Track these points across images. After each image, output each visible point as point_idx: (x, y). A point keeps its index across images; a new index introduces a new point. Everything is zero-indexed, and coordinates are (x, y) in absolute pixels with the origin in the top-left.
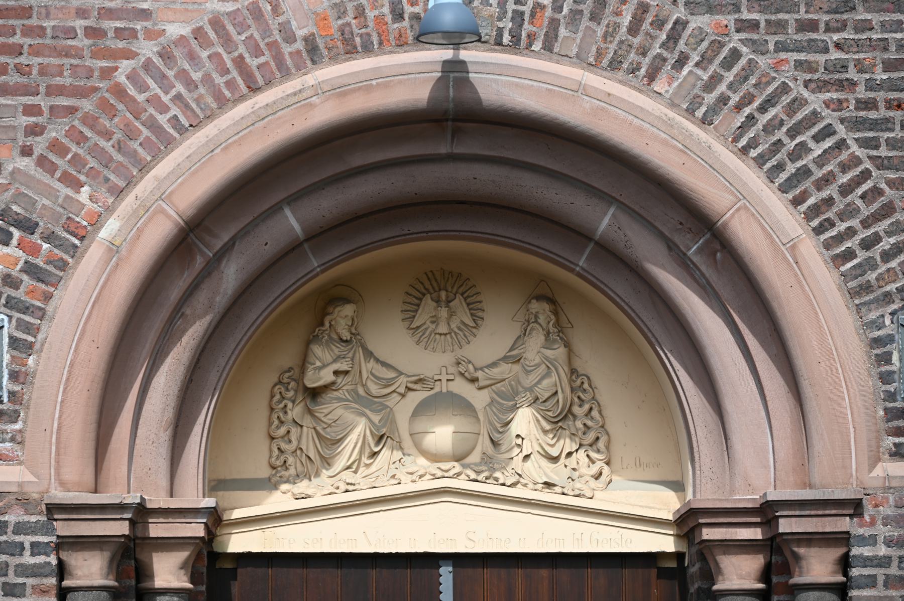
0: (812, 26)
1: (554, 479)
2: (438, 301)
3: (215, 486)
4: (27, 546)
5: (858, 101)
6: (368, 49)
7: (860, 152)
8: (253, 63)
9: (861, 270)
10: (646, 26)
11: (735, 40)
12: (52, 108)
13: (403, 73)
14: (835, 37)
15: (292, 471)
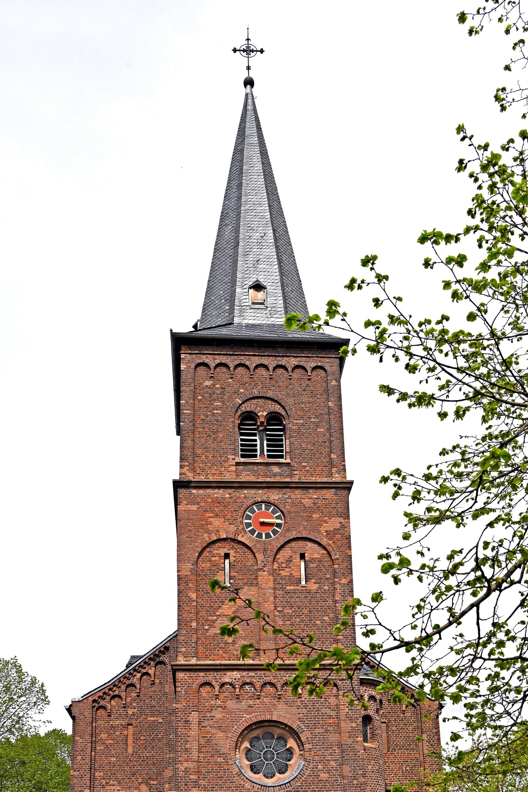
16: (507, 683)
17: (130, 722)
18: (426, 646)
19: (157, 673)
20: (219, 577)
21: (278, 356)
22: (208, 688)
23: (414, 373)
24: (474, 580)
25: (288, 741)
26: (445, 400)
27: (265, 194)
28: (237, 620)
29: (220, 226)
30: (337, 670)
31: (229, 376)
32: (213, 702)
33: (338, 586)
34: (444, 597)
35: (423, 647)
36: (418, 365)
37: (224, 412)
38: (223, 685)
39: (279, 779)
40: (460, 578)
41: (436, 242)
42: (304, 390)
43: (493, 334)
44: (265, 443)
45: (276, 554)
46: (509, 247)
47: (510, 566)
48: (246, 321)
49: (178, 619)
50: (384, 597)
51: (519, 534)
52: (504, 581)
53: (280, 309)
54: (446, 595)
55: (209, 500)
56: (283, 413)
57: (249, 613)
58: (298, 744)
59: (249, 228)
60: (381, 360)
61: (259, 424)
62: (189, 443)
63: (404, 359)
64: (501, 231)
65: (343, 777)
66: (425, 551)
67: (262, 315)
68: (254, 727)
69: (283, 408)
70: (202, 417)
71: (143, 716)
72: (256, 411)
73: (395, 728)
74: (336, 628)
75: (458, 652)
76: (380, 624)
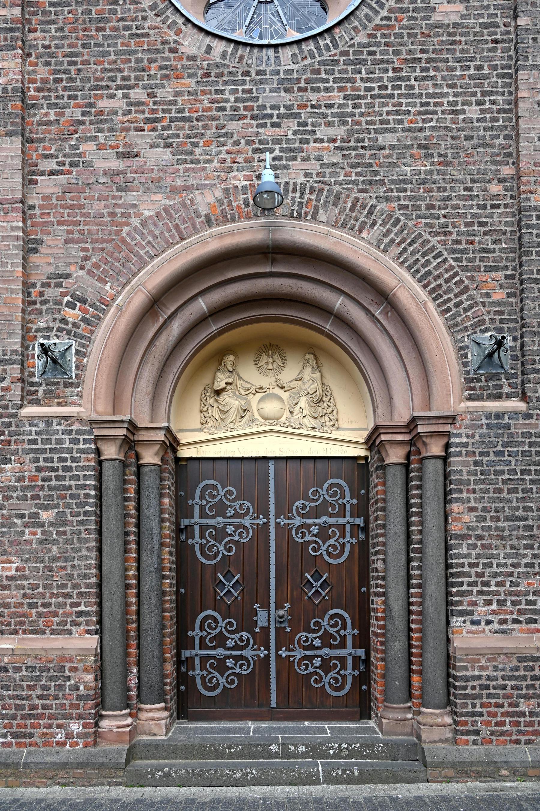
0: (432, 207)
1: (316, 426)
2: (268, 356)
4: (81, 440)
5: (453, 240)
6: (233, 220)
7: (454, 264)
8: (182, 227)
9: (454, 316)
10: (358, 208)
11: (398, 214)
12: (93, 248)
14: (443, 212)
15: (209, 425)
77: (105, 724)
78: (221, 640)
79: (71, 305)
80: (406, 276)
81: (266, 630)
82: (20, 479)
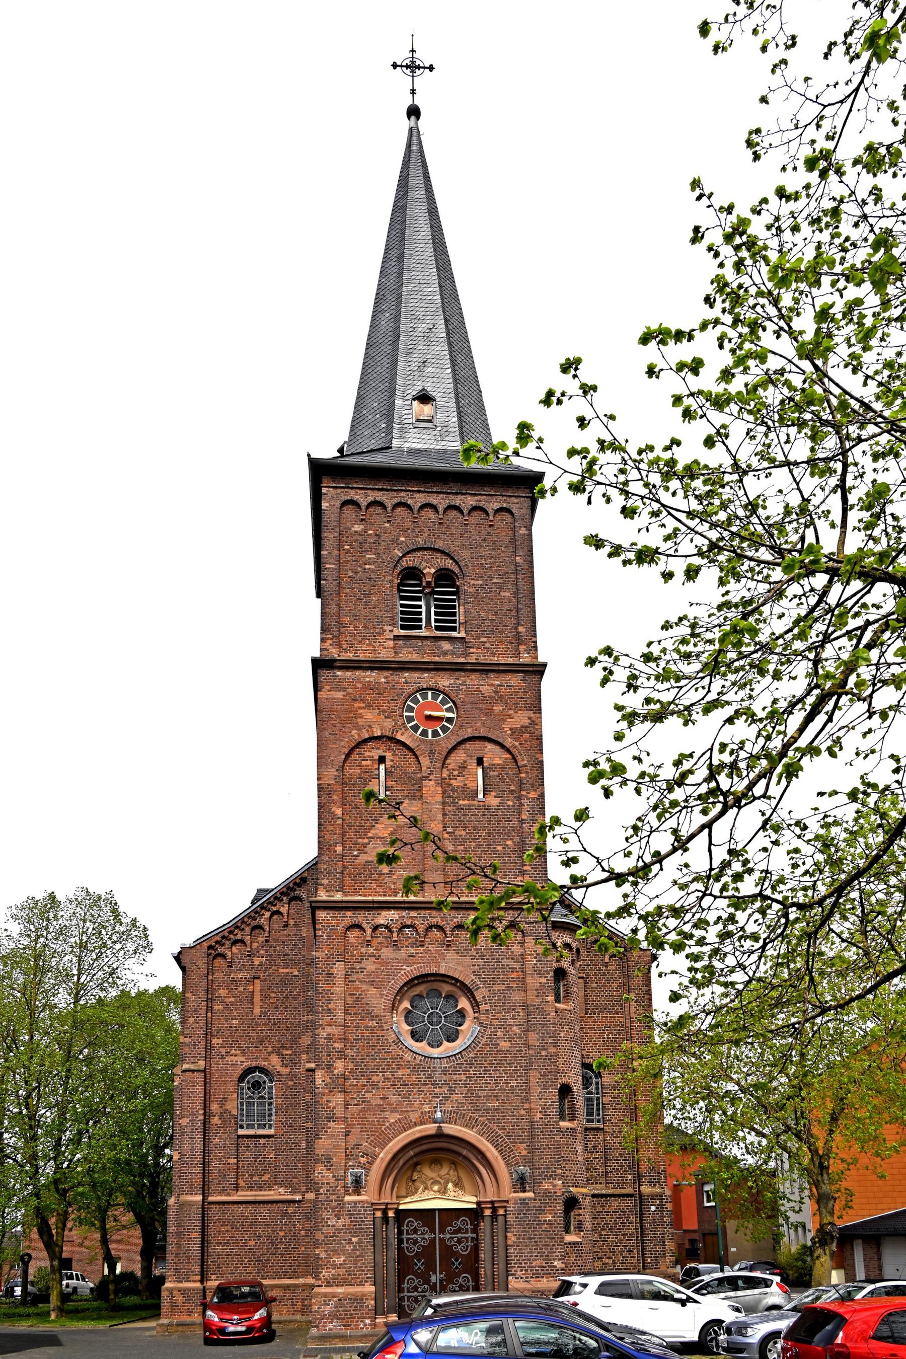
3: (398, 1197)
13: (431, 1128)
16: (742, 929)
17: (257, 975)
18: (643, 879)
19: (292, 911)
20: (372, 786)
21: (450, 493)
22: (357, 932)
23: (632, 518)
24: (706, 793)
25: (459, 1000)
26: (671, 556)
27: (435, 270)
28: (399, 844)
29: (374, 312)
30: (528, 910)
31: (385, 520)
32: (363, 950)
33: (525, 801)
34: (667, 815)
35: (639, 880)
36: (638, 507)
37: (379, 568)
38: (376, 928)
39: (448, 1049)
40: (689, 790)
41: (663, 342)
42: (484, 540)
43: (736, 465)
44: (433, 610)
45: (446, 758)
46: (759, 348)
47: (752, 775)
48: (407, 445)
49: (319, 842)
50: (590, 816)
51: (764, 734)
52: (744, 795)
53: (453, 430)
54: (670, 813)
55: (359, 685)
56: (457, 570)
57: (411, 835)
58: (472, 1004)
59: (413, 317)
60: (589, 502)
61: (424, 584)
62: (333, 608)
63: (619, 501)
64: (749, 326)
65: (529, 1047)
66: (643, 756)
67: (429, 437)
68: (416, 982)
69: (457, 563)
70: (350, 573)
71: (274, 967)
72: (421, 567)
73: (595, 985)
74: (528, 855)
75: (683, 887)
76: (585, 850)
77: (377, 1321)
78: (416, 1289)
79: (362, 1157)
80: (490, 1145)
81: (435, 1284)
82: (344, 1226)
